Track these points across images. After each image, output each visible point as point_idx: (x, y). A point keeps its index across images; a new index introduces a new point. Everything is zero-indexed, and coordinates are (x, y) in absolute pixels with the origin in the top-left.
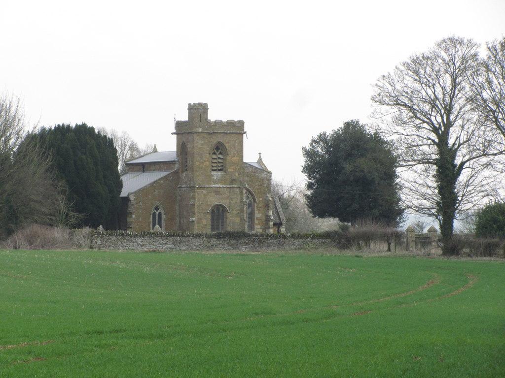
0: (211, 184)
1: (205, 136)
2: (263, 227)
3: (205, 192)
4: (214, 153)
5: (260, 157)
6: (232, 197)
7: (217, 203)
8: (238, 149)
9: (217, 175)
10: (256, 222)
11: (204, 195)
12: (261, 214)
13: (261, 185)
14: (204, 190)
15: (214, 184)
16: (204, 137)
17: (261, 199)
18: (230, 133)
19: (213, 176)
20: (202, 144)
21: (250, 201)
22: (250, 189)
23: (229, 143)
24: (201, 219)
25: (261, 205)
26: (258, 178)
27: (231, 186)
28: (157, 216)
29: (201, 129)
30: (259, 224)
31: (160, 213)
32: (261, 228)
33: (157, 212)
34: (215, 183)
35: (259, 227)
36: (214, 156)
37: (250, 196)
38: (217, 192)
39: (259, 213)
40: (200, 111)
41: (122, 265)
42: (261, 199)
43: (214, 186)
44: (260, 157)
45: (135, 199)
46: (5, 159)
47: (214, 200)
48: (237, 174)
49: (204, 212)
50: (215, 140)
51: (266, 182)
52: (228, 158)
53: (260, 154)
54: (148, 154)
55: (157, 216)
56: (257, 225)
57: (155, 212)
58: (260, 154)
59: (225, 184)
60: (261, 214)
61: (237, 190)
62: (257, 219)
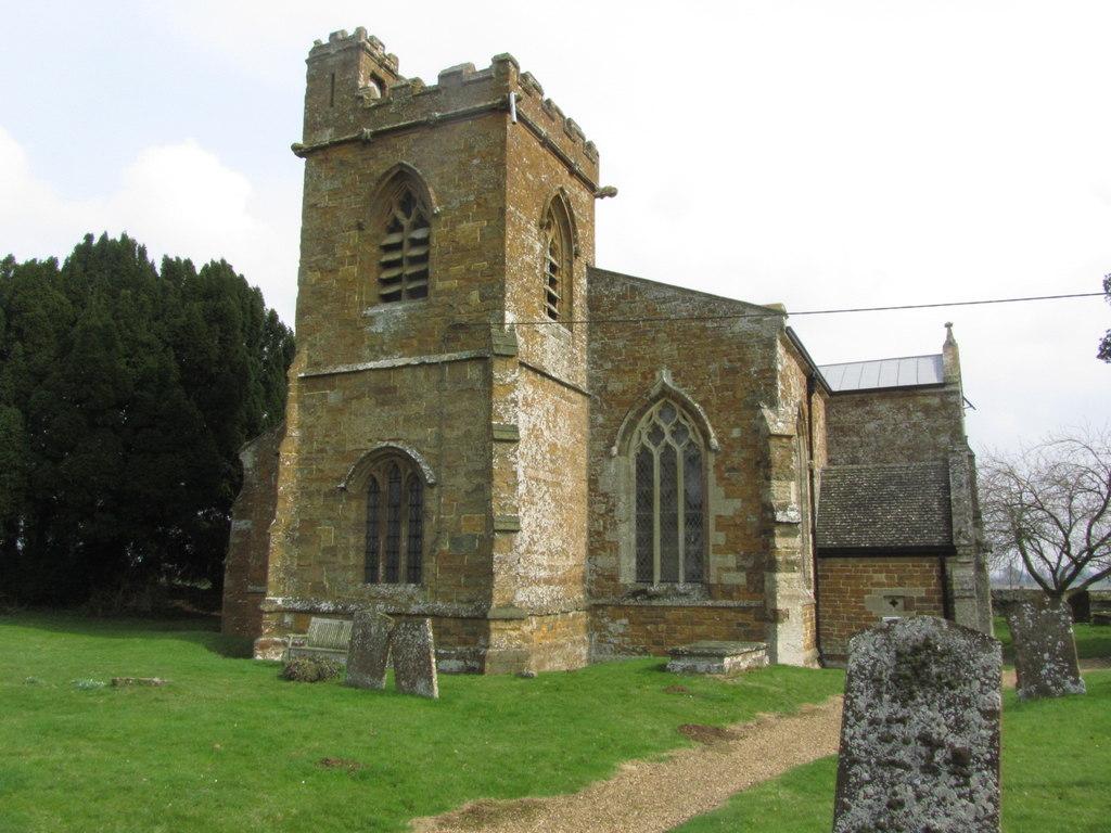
0: (360, 359)
1: (350, 157)
2: (749, 564)
3: (333, 397)
4: (396, 227)
5: (950, 335)
6: (449, 408)
8: (484, 181)
9: (387, 317)
10: (717, 537)
12: (737, 503)
13: (733, 371)
14: (332, 388)
15: (376, 358)
16: (342, 163)
17: (736, 433)
18: (444, 121)
19: (370, 320)
21: (691, 444)
22: (682, 391)
23: (443, 163)
25: (737, 458)
26: (718, 340)
27: (445, 357)
29: (330, 131)
30: (730, 548)
32: (739, 568)
34: (379, 351)
35: (731, 560)
37: (689, 424)
38: (384, 389)
39: (727, 496)
40: (331, 62)
43: (371, 365)
44: (950, 335)
45: (256, 465)
46: (724, 483)
47: (369, 429)
48: (475, 296)
50: (384, 160)
51: (757, 352)
54: (544, 375)
56: (719, 550)
58: (949, 326)
59: (420, 353)
60: (737, 503)
62: (719, 527)
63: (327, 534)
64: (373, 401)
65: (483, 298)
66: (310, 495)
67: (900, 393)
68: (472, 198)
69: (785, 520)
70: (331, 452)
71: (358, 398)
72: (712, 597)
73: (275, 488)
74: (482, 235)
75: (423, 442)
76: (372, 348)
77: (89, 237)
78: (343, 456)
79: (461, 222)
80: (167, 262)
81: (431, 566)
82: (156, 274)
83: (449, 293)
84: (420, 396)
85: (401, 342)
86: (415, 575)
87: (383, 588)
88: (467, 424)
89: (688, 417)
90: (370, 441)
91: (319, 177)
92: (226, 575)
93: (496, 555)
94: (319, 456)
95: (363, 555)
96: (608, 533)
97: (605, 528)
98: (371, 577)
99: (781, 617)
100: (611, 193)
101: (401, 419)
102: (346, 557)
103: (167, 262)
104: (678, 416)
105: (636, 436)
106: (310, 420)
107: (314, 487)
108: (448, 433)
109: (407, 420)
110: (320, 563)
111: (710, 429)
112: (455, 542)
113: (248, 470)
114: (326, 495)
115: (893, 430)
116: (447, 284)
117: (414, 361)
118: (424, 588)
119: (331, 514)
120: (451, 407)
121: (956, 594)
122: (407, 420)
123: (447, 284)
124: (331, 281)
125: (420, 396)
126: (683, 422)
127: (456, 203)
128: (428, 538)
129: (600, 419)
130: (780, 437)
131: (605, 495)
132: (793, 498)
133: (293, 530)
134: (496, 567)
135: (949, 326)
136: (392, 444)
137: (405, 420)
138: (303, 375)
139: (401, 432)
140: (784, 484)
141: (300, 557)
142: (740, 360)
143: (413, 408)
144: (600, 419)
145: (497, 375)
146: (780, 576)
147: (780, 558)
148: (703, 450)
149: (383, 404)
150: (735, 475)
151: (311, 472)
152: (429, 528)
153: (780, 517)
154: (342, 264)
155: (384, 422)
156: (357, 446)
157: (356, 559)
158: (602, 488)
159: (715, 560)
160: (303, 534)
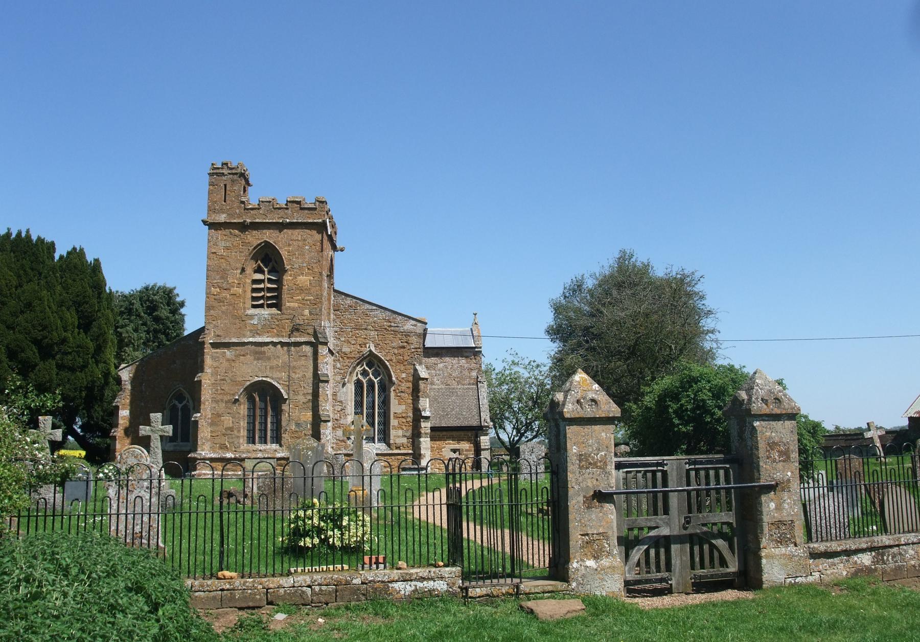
0: (244, 336)
3: (228, 353)
7: (257, 379)
10: (394, 422)
11: (228, 360)
12: (403, 407)
15: (253, 336)
20: (227, 248)
22: (379, 355)
23: (289, 245)
24: (219, 415)
27: (293, 340)
28: (180, 414)
29: (224, 215)
31: (185, 406)
33: (180, 406)
34: (256, 333)
35: (400, 432)
36: (259, 276)
41: (477, 484)
42: (404, 375)
48: (307, 312)
49: (226, 398)
50: (255, 238)
52: (287, 278)
53: (475, 314)
55: (180, 414)
56: (395, 428)
57: (174, 406)
59: (278, 336)
61: (308, 349)
62: (396, 417)
63: (228, 421)
64: (252, 358)
65: (311, 313)
66: (217, 402)
67: (455, 350)
68: (305, 265)
69: (425, 415)
70: (229, 381)
71: (243, 356)
72: (392, 449)
73: (200, 398)
74: (310, 284)
75: (280, 379)
76: (251, 331)
77: (74, 249)
78: (234, 382)
79: (299, 276)
80: (39, 238)
81: (286, 437)
82: (53, 258)
83: (293, 309)
84: (278, 357)
85: (267, 328)
86: (277, 439)
87: (259, 446)
88: (303, 372)
89: (381, 367)
90: (251, 376)
91: (217, 238)
92: (117, 442)
93: (322, 431)
94: (222, 382)
95: (246, 431)
96: (342, 420)
97: (340, 417)
98: (251, 440)
99: (422, 457)
100: (342, 250)
101: (268, 367)
102: (239, 431)
103: (39, 238)
104: (376, 366)
105: (355, 374)
106: (215, 364)
107: (220, 397)
108: (293, 375)
109: (272, 368)
110: (224, 435)
111: (392, 373)
112: (298, 425)
113: (125, 381)
114: (226, 402)
115: (451, 368)
116: (292, 304)
117: (275, 340)
118: (281, 446)
119: (229, 411)
120: (295, 363)
121: (482, 447)
122: (272, 368)
123: (292, 304)
124: (225, 294)
125: (278, 357)
126: (378, 368)
127: (296, 266)
128: (284, 423)
129: (338, 365)
130: (423, 379)
131: (341, 402)
132: (428, 406)
133: (208, 419)
134: (322, 436)
135: (475, 314)
136: (264, 379)
137: (270, 368)
138: (212, 341)
139: (268, 373)
140: (424, 399)
141: (212, 432)
142: (406, 342)
143: (274, 363)
144: (338, 365)
145: (320, 351)
146: (422, 440)
147: (423, 432)
148: (387, 383)
149: (258, 359)
150: (402, 394)
151: (217, 390)
152: (285, 417)
153: (423, 414)
154: (233, 287)
155: (259, 368)
156: (244, 379)
157: (244, 433)
158: (339, 399)
159: (393, 433)
160: (215, 420)
